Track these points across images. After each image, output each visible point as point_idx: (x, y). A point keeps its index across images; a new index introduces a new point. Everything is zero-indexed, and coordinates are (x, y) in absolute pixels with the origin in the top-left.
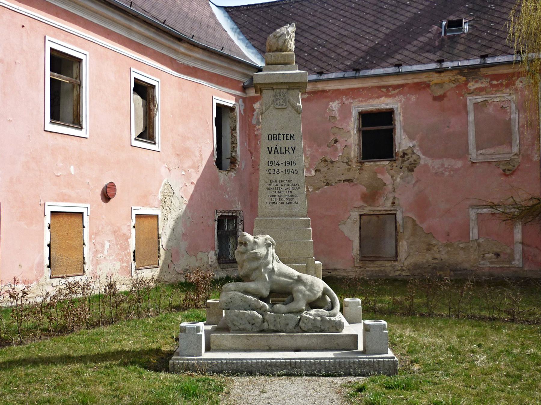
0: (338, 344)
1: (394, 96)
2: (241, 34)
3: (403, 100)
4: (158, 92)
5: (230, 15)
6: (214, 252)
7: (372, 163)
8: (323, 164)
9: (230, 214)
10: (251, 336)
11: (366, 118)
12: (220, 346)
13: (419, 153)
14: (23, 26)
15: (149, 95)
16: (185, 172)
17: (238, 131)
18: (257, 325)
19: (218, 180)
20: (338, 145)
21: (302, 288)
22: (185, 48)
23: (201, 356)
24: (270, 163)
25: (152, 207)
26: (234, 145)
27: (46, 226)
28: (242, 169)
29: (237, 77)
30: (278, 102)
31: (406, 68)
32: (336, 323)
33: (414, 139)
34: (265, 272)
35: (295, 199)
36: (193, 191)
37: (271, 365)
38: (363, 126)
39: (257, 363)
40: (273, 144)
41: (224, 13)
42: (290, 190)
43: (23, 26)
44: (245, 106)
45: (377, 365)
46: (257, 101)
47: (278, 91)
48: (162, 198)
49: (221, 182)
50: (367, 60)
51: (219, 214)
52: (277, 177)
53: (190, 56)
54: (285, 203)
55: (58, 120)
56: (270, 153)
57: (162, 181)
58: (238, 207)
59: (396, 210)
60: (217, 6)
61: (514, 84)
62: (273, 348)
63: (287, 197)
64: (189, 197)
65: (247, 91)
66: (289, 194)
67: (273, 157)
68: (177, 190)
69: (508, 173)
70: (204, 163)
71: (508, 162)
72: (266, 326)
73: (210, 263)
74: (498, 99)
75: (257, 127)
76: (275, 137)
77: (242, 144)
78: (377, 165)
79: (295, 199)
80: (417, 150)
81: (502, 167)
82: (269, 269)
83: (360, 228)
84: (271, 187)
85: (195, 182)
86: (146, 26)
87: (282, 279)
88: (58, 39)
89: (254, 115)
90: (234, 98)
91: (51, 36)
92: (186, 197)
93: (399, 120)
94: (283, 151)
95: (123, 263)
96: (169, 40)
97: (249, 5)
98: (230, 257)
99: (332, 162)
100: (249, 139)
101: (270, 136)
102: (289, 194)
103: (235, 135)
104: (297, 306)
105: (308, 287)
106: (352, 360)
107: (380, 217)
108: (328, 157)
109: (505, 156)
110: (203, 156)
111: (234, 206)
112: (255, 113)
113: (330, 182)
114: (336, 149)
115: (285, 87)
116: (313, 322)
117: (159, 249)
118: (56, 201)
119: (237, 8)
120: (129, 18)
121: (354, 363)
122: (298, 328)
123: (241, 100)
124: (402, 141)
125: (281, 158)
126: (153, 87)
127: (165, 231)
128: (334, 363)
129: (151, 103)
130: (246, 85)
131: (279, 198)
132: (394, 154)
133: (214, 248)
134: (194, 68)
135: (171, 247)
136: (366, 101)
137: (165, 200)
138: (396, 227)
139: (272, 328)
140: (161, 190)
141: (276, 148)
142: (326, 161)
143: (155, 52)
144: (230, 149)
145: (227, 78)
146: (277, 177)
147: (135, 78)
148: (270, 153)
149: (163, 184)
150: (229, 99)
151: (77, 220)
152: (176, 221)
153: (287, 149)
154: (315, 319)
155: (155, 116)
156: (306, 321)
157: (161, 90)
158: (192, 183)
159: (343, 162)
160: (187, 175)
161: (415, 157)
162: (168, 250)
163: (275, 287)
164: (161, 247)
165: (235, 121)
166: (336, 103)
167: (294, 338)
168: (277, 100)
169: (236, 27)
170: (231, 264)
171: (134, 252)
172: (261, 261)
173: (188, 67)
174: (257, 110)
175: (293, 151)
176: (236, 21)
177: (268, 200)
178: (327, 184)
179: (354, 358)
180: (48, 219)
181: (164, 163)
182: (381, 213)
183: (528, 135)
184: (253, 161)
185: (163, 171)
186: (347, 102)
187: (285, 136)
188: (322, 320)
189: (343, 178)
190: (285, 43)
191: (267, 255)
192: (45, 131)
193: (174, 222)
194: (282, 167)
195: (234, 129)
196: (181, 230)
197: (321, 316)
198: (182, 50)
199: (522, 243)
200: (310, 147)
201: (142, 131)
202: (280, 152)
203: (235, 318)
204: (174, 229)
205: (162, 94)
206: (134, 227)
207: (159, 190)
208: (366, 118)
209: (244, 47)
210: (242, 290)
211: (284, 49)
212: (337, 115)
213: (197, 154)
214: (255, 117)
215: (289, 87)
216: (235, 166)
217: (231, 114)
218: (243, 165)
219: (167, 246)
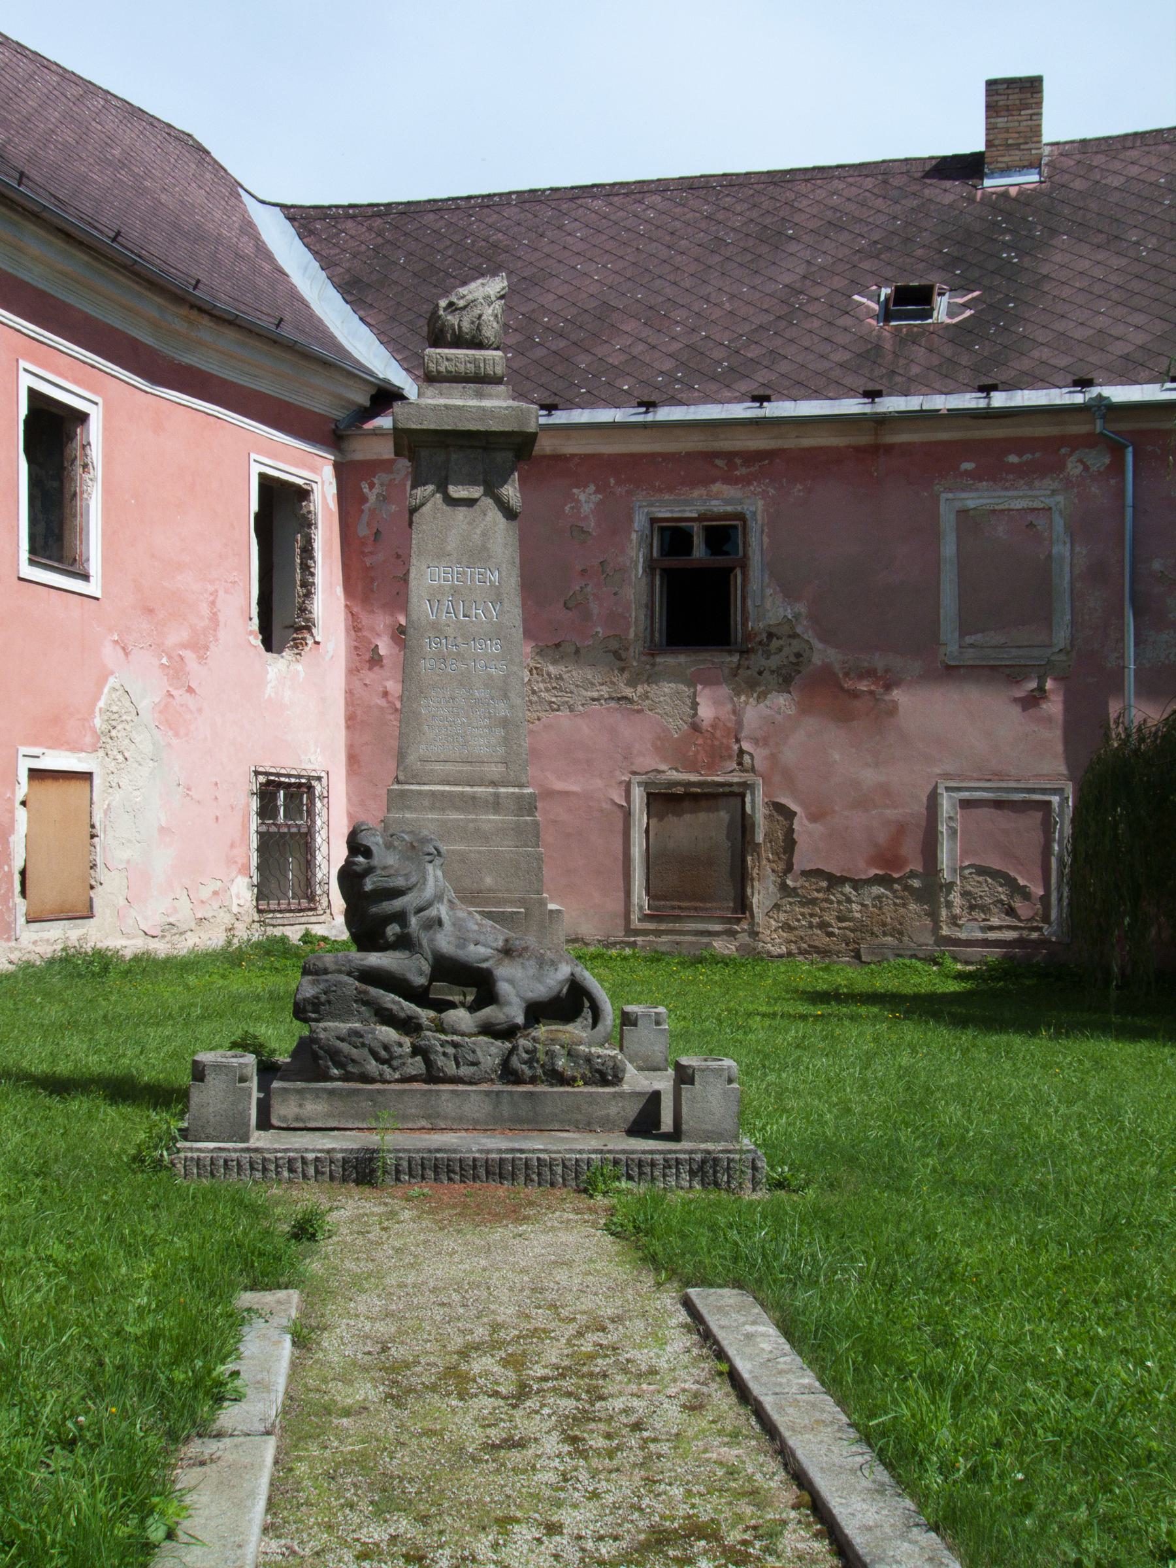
11: (673, 538)
50: (678, 380)
97: (814, 168)
126: (83, 418)
149: (106, 690)
157: (105, 429)
161: (796, 646)
171: (23, 873)
206: (24, 803)
207: (95, 705)
208: (673, 538)
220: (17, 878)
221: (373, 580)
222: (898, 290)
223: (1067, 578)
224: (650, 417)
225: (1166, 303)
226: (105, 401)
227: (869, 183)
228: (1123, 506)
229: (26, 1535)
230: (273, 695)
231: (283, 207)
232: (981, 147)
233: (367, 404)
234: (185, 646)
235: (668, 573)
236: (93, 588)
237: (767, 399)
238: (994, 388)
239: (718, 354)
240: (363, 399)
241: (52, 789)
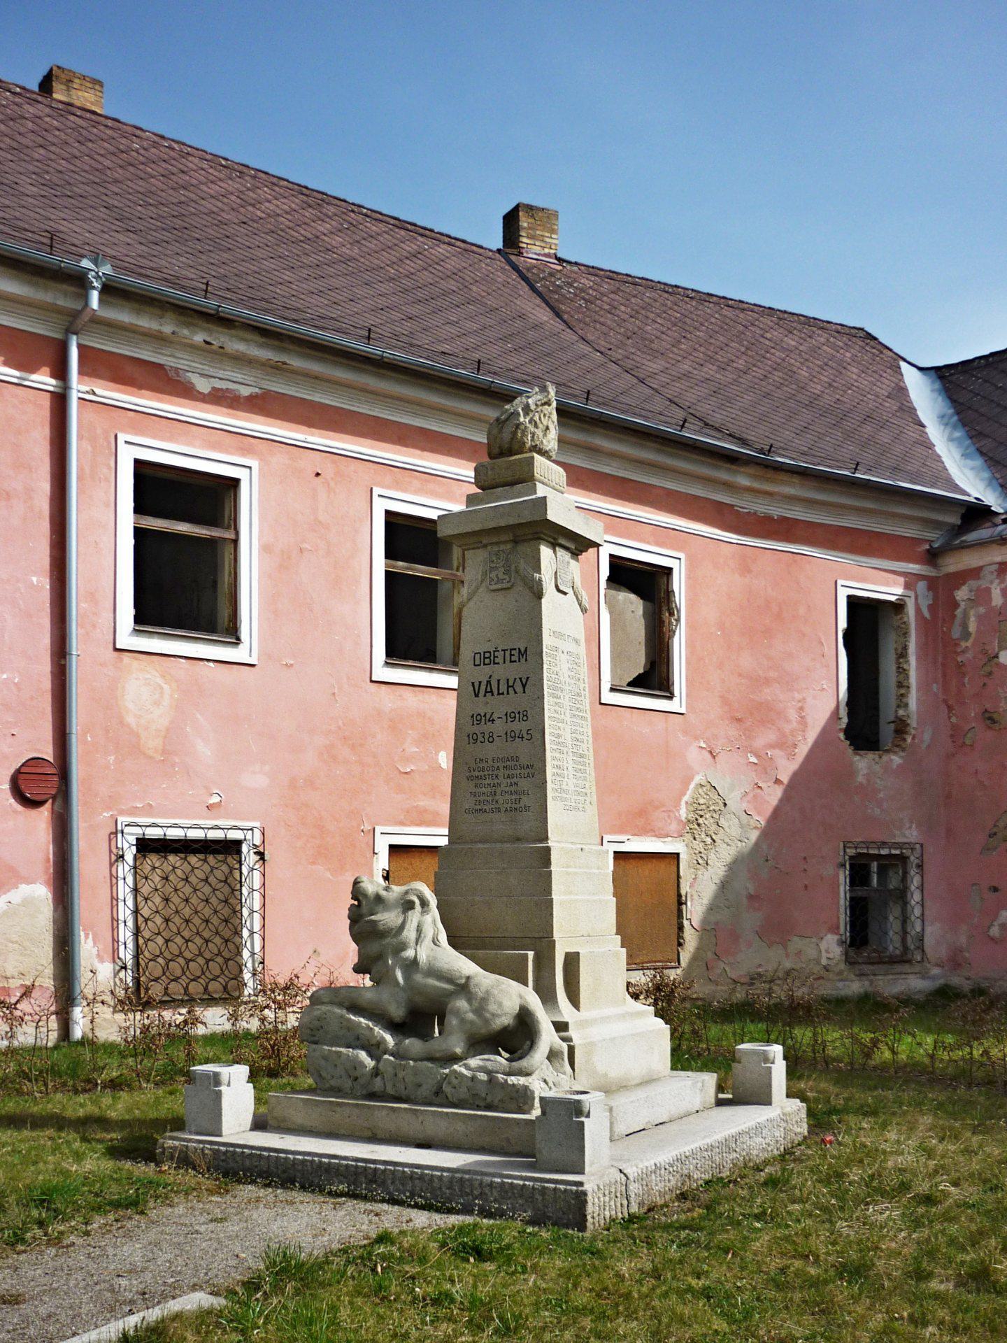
0: (508, 1140)
2: (960, 425)
4: (679, 585)
5: (944, 386)
6: (836, 937)
9: (884, 852)
10: (338, 1104)
12: (284, 1120)
14: (318, 474)
15: (660, 590)
16: (757, 756)
17: (913, 659)
18: (362, 1081)
19: (851, 772)
21: (462, 1004)
22: (750, 476)
23: (220, 1136)
25: (660, 835)
26: (903, 691)
28: (924, 746)
29: (909, 531)
30: (493, 575)
32: (517, 1091)
34: (394, 965)
36: (781, 801)
37: (328, 1169)
39: (304, 1161)
41: (933, 382)
42: (515, 780)
43: (318, 474)
44: (936, 598)
45: (540, 1198)
46: (964, 584)
47: (496, 548)
48: (691, 816)
49: (860, 779)
51: (851, 852)
52: (490, 751)
53: (770, 494)
54: (503, 810)
55: (434, 661)
56: (477, 695)
57: (691, 779)
58: (912, 834)
60: (920, 369)
62: (380, 1135)
63: (507, 797)
64: (769, 810)
65: (940, 561)
66: (512, 789)
68: (734, 800)
70: (812, 735)
72: (378, 1084)
73: (824, 962)
75: (964, 644)
77: (924, 687)
82: (406, 959)
84: (477, 773)
85: (785, 779)
86: (633, 439)
87: (432, 982)
89: (954, 617)
90: (901, 580)
92: (759, 814)
96: (703, 463)
97: (992, 354)
98: (891, 948)
100: (944, 675)
101: (477, 657)
102: (512, 789)
103: (905, 666)
104: (444, 1047)
105: (476, 1004)
106: (488, 1179)
110: (809, 720)
111: (897, 832)
112: (959, 612)
115: (504, 537)
116: (470, 1084)
117: (681, 928)
118: (402, 824)
119: (965, 366)
120: (586, 426)
121: (491, 1185)
122: (438, 1096)
123: (922, 586)
126: (668, 571)
127: (700, 891)
128: (451, 1180)
129: (665, 608)
130: (936, 545)
131: (490, 798)
133: (838, 928)
134: (784, 519)
135: (717, 923)
137: (701, 821)
139: (390, 1090)
140: (686, 798)
141: (489, 682)
143: (670, 493)
144: (893, 702)
145: (879, 535)
146: (490, 751)
147: (611, 556)
148: (477, 695)
149: (692, 786)
150: (887, 584)
152: (733, 867)
153: (511, 683)
154: (473, 1078)
155: (671, 637)
156: (455, 1081)
157: (688, 577)
158: (777, 781)
160: (764, 766)
162: (709, 930)
163: (418, 999)
164: (686, 923)
165: (906, 634)
167: (421, 1118)
168: (492, 569)
169: (951, 411)
170: (886, 966)
172: (388, 940)
173: (769, 518)
174: (963, 605)
175: (524, 686)
176: (955, 397)
179: (494, 1175)
181: (696, 738)
184: (955, 727)
185: (695, 755)
187: (508, 653)
188: (490, 1081)
190: (515, 433)
191: (402, 927)
192: (372, 681)
193: (724, 869)
194: (499, 727)
195: (902, 655)
196: (745, 885)
197: (489, 1073)
198: (744, 481)
201: (642, 671)
202: (495, 692)
203: (323, 1062)
204: (724, 886)
205: (688, 587)
207: (680, 800)
209: (957, 455)
210: (347, 1004)
211: (516, 447)
213: (793, 715)
214: (958, 621)
215: (515, 536)
216: (905, 740)
217: (896, 620)
218: (927, 737)
219: (705, 921)
221: (964, 675)
225: (999, 405)
226: (689, 558)
230: (864, 782)
233: (959, 522)
234: (772, 746)
240: (954, 519)
241: (631, 865)
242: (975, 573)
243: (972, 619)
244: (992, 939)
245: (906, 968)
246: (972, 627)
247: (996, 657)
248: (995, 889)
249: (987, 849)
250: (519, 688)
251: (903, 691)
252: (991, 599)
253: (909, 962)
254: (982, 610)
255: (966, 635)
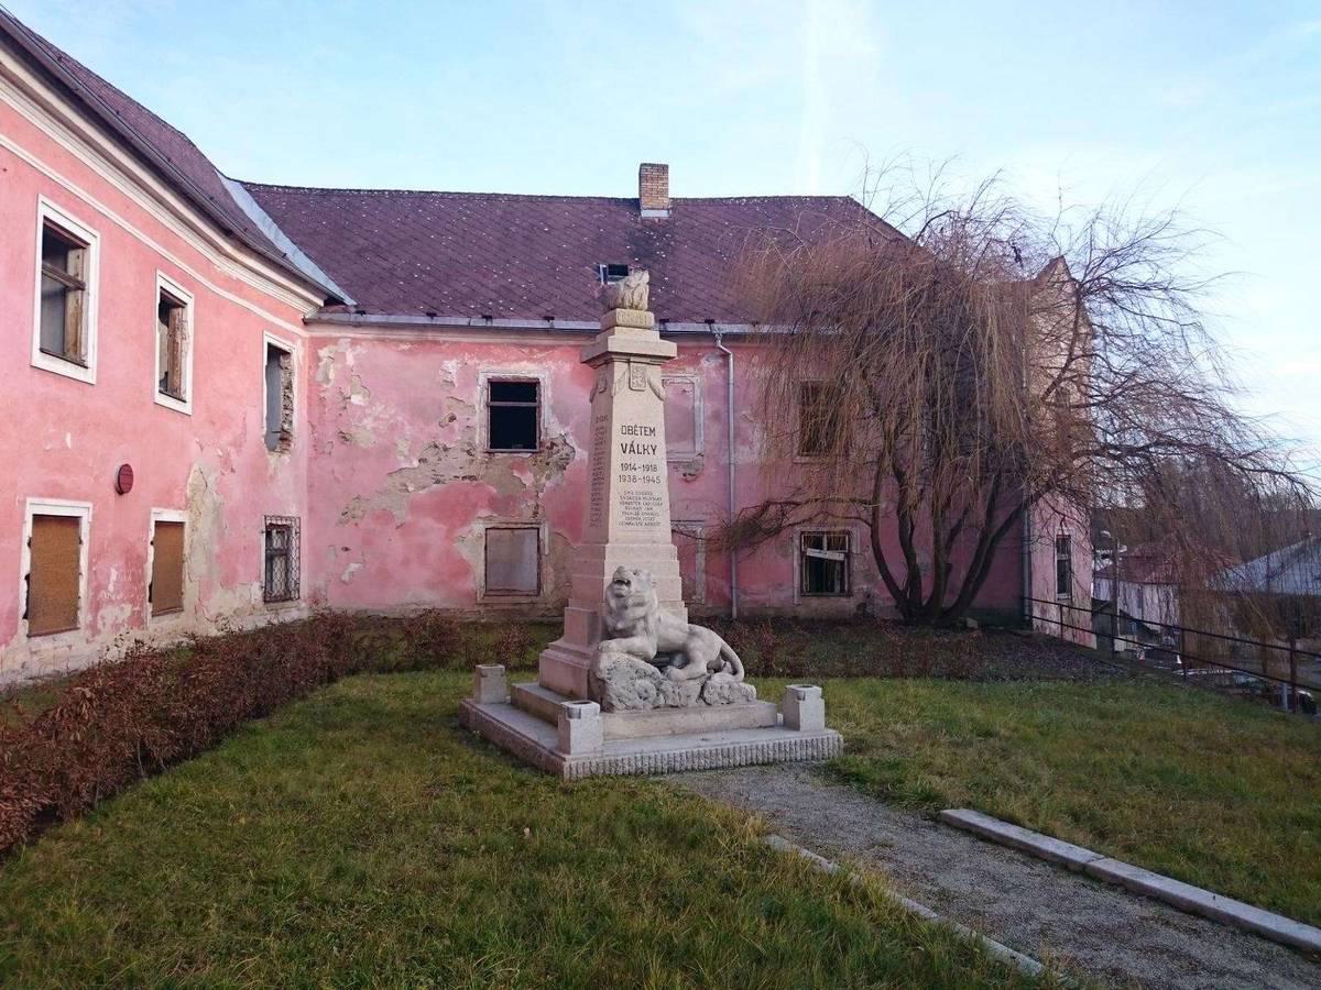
1: (540, 361)
3: (553, 368)
7: (505, 455)
8: (433, 451)
11: (499, 389)
13: (573, 444)
20: (455, 424)
24: (625, 466)
26: (288, 412)
27: (26, 540)
31: (559, 324)
33: (567, 425)
35: (657, 519)
38: (492, 400)
40: (628, 439)
43: (5, 170)
46: (325, 346)
50: (501, 305)
51: (268, 522)
52: (634, 487)
53: (236, 261)
58: (292, 511)
59: (540, 523)
61: (699, 363)
67: (628, 458)
69: (689, 478)
71: (689, 465)
74: (679, 380)
75: (325, 386)
76: (631, 430)
78: (511, 458)
79: (657, 519)
80: (571, 440)
81: (682, 471)
83: (486, 549)
88: (56, 202)
89: (318, 367)
91: (46, 196)
93: (547, 396)
94: (641, 450)
95: (134, 606)
99: (446, 449)
107: (516, 532)
108: (441, 441)
109: (688, 456)
113: (442, 479)
114: (452, 431)
124: (550, 425)
125: (639, 460)
132: (537, 444)
136: (498, 364)
138: (539, 547)
142: (436, 446)
146: (634, 487)
151: (69, 530)
159: (463, 450)
161: (567, 450)
166: (454, 362)
171: (150, 587)
174: (325, 360)
177: (623, 519)
178: (438, 482)
180: (28, 530)
182: (519, 526)
183: (715, 429)
186: (469, 362)
189: (461, 473)
194: (639, 473)
199: (706, 572)
200: (411, 424)
206: (152, 543)
208: (499, 389)
212: (455, 381)
214: (321, 370)
220: (148, 589)
221: (325, 406)
222: (610, 267)
223: (702, 418)
224: (489, 324)
227: (583, 208)
228: (729, 384)
229: (1078, 947)
231: (242, 183)
232: (636, 195)
235: (492, 407)
236: (187, 408)
237: (435, 315)
238: (667, 321)
239: (520, 292)
242: (335, 341)
243: (332, 370)
244: (344, 582)
245: (288, 603)
246: (332, 375)
247: (350, 398)
248: (347, 549)
249: (337, 525)
250: (651, 451)
251: (288, 412)
252: (345, 360)
253: (291, 599)
254: (339, 366)
255: (327, 380)
